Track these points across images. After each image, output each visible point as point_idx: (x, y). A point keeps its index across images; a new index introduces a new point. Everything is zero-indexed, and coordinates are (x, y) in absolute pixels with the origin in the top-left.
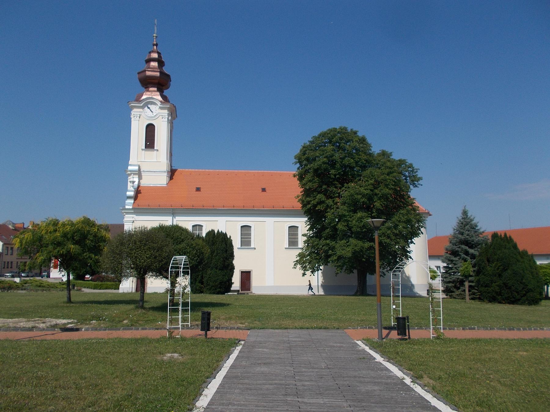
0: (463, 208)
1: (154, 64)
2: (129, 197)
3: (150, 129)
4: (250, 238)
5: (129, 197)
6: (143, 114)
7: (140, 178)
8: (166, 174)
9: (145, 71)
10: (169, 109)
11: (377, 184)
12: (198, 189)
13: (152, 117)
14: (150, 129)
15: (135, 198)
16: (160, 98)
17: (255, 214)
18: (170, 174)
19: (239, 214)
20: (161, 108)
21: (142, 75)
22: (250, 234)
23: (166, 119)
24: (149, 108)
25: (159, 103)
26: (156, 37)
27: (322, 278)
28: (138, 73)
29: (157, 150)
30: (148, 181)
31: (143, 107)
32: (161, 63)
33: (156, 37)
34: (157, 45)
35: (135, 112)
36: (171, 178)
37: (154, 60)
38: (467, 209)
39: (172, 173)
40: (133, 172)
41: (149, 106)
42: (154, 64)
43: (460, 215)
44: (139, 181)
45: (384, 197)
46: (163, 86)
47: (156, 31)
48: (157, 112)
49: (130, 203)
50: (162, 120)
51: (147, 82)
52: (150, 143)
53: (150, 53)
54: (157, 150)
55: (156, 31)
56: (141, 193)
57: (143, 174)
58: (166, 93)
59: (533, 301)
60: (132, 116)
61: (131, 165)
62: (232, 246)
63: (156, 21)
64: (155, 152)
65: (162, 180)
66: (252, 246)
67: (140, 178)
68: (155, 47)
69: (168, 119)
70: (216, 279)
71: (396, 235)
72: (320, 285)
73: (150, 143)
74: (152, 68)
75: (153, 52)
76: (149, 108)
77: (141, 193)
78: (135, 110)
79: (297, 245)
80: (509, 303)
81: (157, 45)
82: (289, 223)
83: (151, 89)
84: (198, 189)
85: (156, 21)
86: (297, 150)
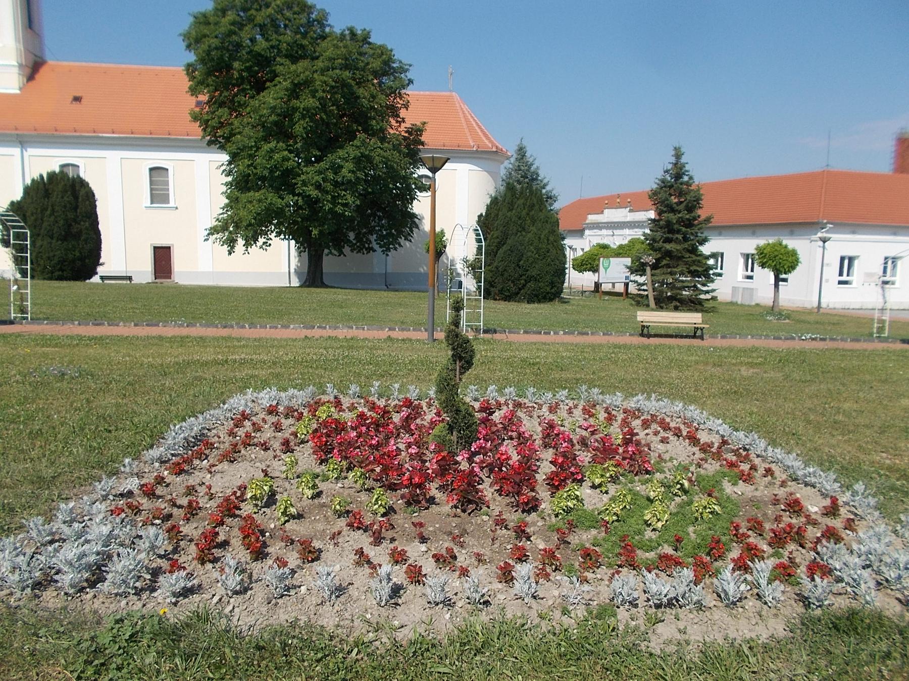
0: (519, 142)
4: (168, 190)
11: (295, 91)
17: (463, 158)
19: (139, 145)
22: (167, 183)
27: (297, 259)
36: (31, 78)
38: (525, 143)
43: (668, 160)
45: (308, 113)
59: (536, 296)
66: (172, 204)
70: (51, 254)
71: (336, 184)
72: (292, 271)
79: (168, 203)
80: (539, 302)
82: (151, 161)
86: (186, 23)
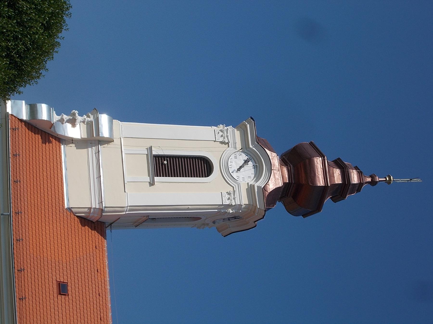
1: (337, 177)
2: (33, 110)
3: (199, 167)
5: (33, 110)
6: (231, 150)
7: (81, 144)
8: (95, 205)
9: (322, 156)
10: (251, 207)
12: (62, 289)
13: (227, 168)
14: (199, 167)
15: (33, 126)
16: (271, 187)
18: (95, 217)
20: (250, 189)
21: (311, 150)
23: (228, 202)
24: (246, 162)
25: (261, 183)
26: (389, 182)
28: (311, 144)
29: (152, 184)
30: (71, 159)
31: (245, 149)
32: (342, 190)
33: (389, 182)
34: (373, 183)
35: (234, 135)
36: (85, 221)
37: (345, 176)
39: (96, 223)
40: (93, 127)
41: (250, 163)
42: (337, 177)
44: (72, 141)
46: (295, 197)
47: (400, 180)
48: (240, 180)
49: (20, 110)
50: (224, 193)
51: (297, 161)
52: (167, 166)
53: (356, 168)
54: (152, 184)
55: (400, 180)
56: (44, 142)
57: (91, 151)
58: (279, 206)
60: (221, 127)
61: (64, 147)
62: (276, 188)
63: (419, 180)
64: (148, 179)
65: (78, 195)
67: (81, 144)
68: (369, 180)
69: (229, 206)
73: (167, 166)
74: (331, 172)
75: (360, 173)
76: (246, 162)
77: (44, 142)
78: (237, 133)
81: (373, 183)
83: (285, 170)
84: (62, 289)
85: (419, 180)
